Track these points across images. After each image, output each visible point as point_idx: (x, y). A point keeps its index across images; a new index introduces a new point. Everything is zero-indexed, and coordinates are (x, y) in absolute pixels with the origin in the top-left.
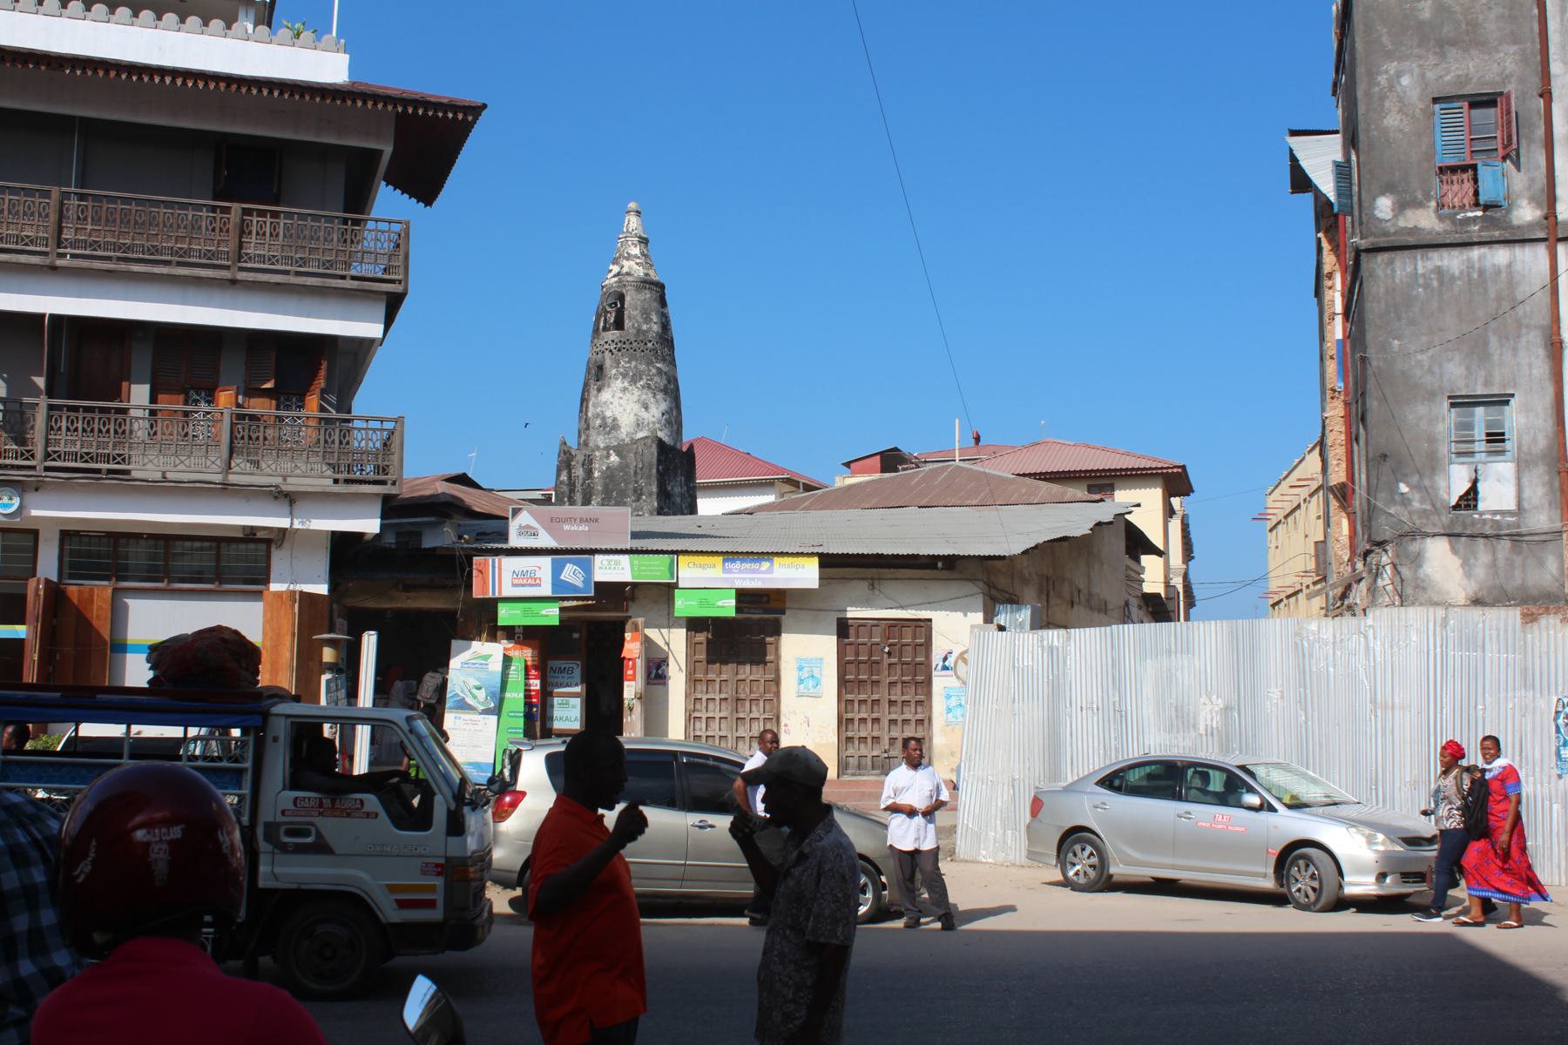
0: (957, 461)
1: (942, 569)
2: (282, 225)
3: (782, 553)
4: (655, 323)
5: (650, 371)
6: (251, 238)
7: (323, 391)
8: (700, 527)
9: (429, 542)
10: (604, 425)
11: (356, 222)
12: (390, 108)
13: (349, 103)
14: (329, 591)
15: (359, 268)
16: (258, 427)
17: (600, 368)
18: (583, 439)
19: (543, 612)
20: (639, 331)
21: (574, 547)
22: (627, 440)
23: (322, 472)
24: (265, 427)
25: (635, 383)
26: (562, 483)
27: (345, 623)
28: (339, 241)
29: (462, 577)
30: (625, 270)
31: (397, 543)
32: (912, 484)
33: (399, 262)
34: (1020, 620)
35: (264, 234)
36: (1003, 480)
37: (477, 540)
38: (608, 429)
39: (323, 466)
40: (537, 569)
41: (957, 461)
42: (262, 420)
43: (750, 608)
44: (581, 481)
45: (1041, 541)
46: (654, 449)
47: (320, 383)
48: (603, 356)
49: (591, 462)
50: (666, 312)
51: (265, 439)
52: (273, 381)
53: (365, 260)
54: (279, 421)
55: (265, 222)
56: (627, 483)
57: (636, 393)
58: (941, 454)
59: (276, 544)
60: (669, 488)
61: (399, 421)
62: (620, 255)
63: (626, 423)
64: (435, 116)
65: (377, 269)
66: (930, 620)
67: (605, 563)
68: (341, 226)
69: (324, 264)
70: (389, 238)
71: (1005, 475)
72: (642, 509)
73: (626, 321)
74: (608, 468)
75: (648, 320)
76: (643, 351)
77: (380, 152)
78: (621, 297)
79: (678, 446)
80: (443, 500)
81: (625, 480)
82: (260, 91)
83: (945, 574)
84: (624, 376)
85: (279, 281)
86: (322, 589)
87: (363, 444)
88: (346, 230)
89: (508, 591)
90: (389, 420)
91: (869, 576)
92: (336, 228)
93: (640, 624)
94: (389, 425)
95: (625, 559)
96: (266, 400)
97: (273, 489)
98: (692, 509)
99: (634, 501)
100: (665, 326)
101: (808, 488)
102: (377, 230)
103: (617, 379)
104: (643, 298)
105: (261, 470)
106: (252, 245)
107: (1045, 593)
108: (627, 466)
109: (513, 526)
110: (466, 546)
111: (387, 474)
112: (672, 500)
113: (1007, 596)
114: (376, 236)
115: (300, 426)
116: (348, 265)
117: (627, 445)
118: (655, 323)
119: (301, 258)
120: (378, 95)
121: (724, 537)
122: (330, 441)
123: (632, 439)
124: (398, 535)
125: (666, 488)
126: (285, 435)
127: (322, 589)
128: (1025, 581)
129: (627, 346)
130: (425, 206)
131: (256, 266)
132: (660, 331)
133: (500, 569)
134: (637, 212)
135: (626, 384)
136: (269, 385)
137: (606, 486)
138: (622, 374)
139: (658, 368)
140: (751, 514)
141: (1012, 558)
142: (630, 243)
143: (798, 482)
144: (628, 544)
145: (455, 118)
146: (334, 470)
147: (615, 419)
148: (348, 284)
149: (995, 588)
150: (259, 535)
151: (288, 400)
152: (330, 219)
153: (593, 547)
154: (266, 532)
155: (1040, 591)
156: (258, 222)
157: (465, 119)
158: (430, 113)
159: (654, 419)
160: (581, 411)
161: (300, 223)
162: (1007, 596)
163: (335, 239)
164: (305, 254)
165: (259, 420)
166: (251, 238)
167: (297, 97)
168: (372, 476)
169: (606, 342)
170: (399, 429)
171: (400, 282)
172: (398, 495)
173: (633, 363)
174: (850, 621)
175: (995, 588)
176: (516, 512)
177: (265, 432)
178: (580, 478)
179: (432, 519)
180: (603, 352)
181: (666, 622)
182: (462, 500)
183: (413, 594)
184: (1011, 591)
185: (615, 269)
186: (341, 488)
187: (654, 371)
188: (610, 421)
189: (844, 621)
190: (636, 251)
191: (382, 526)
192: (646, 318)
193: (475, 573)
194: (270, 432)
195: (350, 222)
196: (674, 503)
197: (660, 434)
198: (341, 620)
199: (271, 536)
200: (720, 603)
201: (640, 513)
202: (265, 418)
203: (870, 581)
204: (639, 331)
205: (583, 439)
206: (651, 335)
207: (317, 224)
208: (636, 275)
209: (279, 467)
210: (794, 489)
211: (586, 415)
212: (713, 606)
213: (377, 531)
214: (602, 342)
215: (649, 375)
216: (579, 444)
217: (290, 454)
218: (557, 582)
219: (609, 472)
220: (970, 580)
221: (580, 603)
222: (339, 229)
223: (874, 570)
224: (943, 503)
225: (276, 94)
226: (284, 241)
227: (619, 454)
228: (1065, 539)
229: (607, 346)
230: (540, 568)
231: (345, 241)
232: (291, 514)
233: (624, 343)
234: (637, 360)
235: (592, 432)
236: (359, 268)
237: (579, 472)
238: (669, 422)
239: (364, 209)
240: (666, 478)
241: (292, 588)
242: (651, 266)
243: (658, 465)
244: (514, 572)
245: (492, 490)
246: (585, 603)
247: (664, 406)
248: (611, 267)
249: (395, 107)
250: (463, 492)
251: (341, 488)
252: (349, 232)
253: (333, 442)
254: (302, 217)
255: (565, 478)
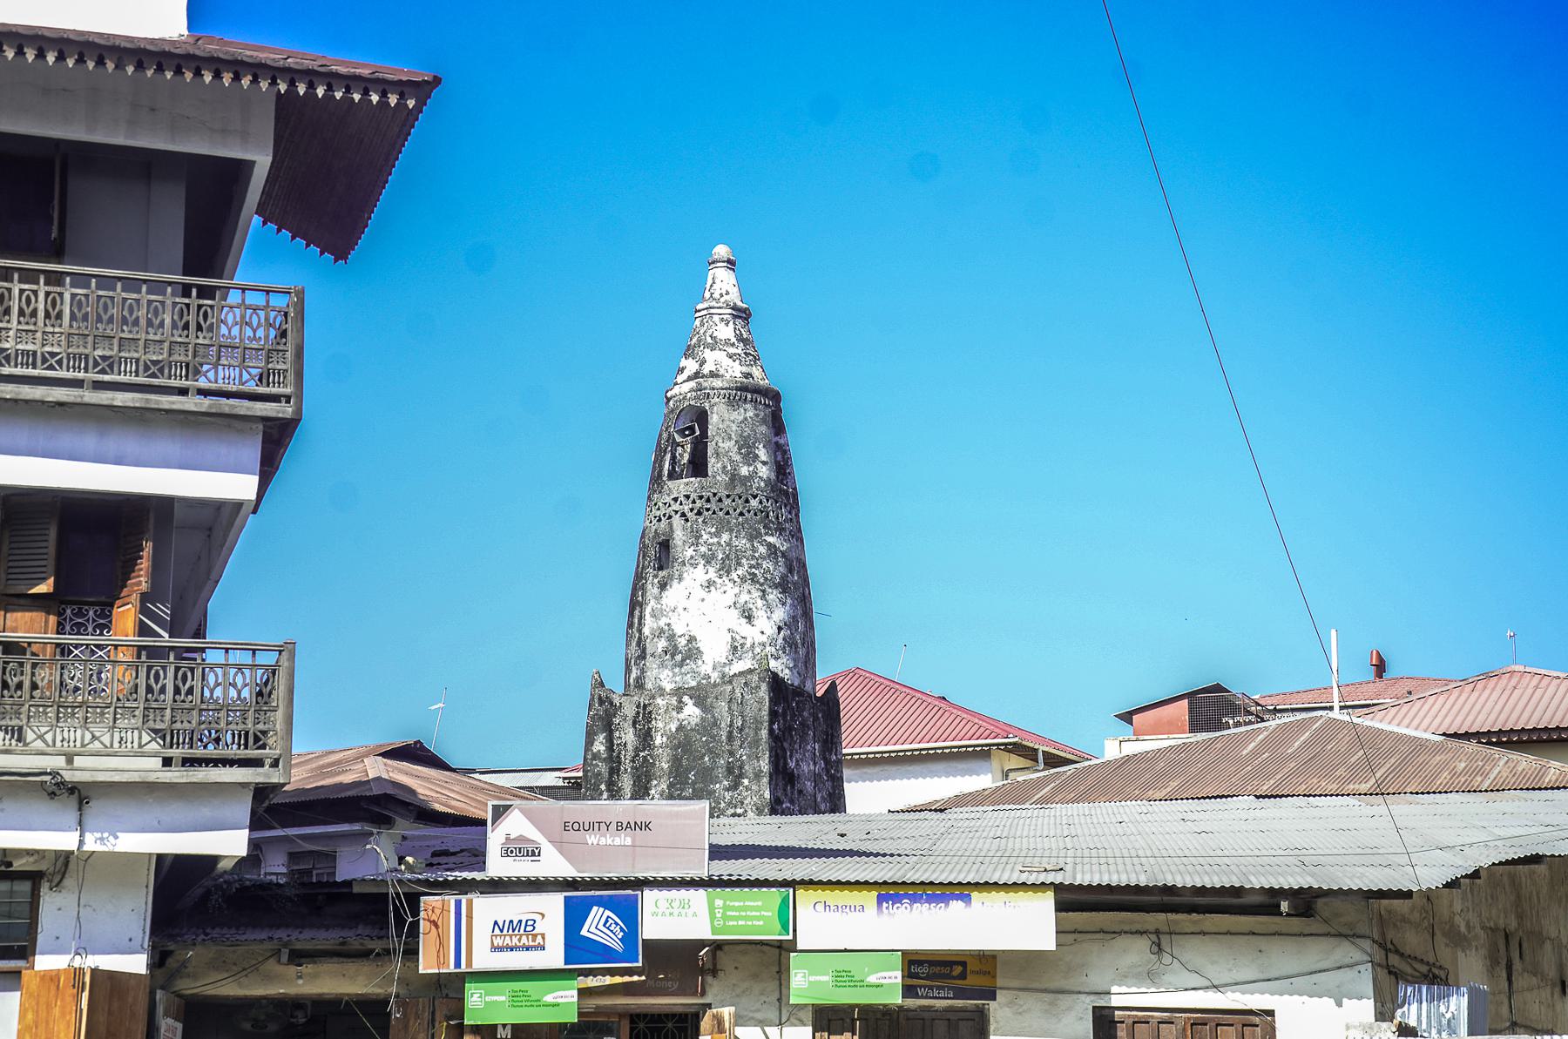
0: (1336, 708)
1: (1288, 915)
2: (67, 297)
3: (987, 883)
4: (764, 463)
5: (754, 550)
6: (8, 322)
7: (145, 598)
8: (843, 835)
9: (347, 870)
10: (672, 651)
11: (206, 292)
12: (264, 85)
13: (189, 76)
14: (151, 966)
15: (211, 375)
16: (21, 665)
17: (665, 545)
18: (633, 675)
19: (549, 998)
20: (734, 478)
21: (606, 875)
22: (715, 677)
23: (140, 746)
24: (34, 666)
25: (728, 572)
26: (596, 756)
27: (180, 1026)
28: (174, 325)
29: (399, 936)
30: (706, 370)
31: (291, 873)
32: (1245, 752)
33: (284, 364)
34: (1448, 1015)
35: (34, 313)
36: (1419, 745)
37: (430, 865)
38: (678, 658)
39: (144, 733)
40: (538, 917)
41: (1336, 708)
42: (28, 653)
43: (931, 988)
44: (630, 754)
45: (1485, 862)
46: (764, 692)
47: (140, 583)
48: (671, 525)
49: (648, 717)
50: (782, 441)
51: (34, 686)
52: (52, 580)
53: (224, 361)
54: (62, 654)
55: (35, 293)
56: (715, 755)
57: (729, 592)
58: (1310, 696)
59: (50, 881)
60: (792, 764)
61: (286, 649)
62: (699, 341)
63: (714, 651)
64: (347, 100)
65: (246, 376)
66: (1271, 1013)
67: (663, 905)
68: (177, 300)
69: (147, 368)
70: (267, 318)
71: (1428, 736)
72: (742, 803)
73: (712, 461)
74: (680, 728)
75: (750, 458)
76: (741, 514)
77: (250, 165)
78: (702, 417)
79: (808, 687)
80: (376, 791)
81: (710, 751)
82: (20, 52)
83: (1296, 924)
84: (709, 560)
85: (64, 399)
86: (136, 964)
87: (218, 692)
88: (188, 306)
89: (484, 958)
90: (267, 649)
91: (1152, 928)
92: (169, 302)
93: (726, 1018)
94: (268, 659)
95: (699, 896)
96: (37, 617)
97: (47, 778)
98: (836, 804)
99: (728, 790)
100: (782, 467)
101: (1053, 761)
102: (243, 305)
103: (695, 566)
104: (741, 418)
105: (26, 745)
106: (11, 333)
107: (1504, 963)
108: (715, 724)
109: (495, 839)
110: (408, 876)
111: (263, 747)
112: (797, 786)
113: (1424, 969)
114: (243, 317)
115: (102, 662)
116: (193, 371)
117: (715, 685)
118: (764, 463)
119: (104, 358)
120: (242, 63)
121: (884, 855)
122: (157, 688)
123: (724, 676)
124: (294, 857)
125: (786, 763)
126: (72, 679)
127: (136, 964)
128: (1459, 940)
129: (713, 505)
130: (336, 261)
131: (19, 371)
132: (773, 476)
133: (470, 917)
134: (729, 261)
135: (712, 575)
136: (44, 588)
137: (676, 761)
138: (703, 556)
139: (770, 545)
140: (941, 811)
141: (1428, 895)
142: (716, 318)
143: (1036, 750)
144: (703, 868)
145: (383, 103)
146: (164, 741)
147: (692, 639)
148: (191, 403)
149: (1397, 952)
150: (18, 865)
151: (80, 614)
152: (157, 287)
153: (641, 875)
154: (31, 859)
155: (1493, 961)
156: (22, 291)
157: (401, 104)
158: (338, 95)
159: (764, 639)
160: (630, 625)
161: (101, 293)
162: (1424, 969)
163: (168, 321)
164: (111, 349)
165: (23, 651)
166: (8, 322)
167: (91, 65)
168: (234, 751)
169: (675, 500)
170: (284, 662)
171: (288, 399)
172: (284, 785)
173: (725, 537)
174: (1117, 1013)
175: (1397, 952)
176: (499, 812)
177: (33, 674)
178: (630, 747)
179: (356, 827)
180: (670, 517)
181: (773, 1015)
182: (413, 792)
183: (308, 969)
184: (1432, 960)
185: (691, 366)
186: (176, 775)
187: (762, 550)
188: (682, 642)
189: (1106, 1012)
190: (726, 332)
191: (254, 844)
192: (749, 453)
193: (423, 926)
194: (43, 675)
195: (194, 292)
196: (800, 792)
197: (773, 664)
198: (170, 1021)
199: (42, 867)
200: (872, 979)
201: (739, 811)
202: (34, 648)
203: (1154, 937)
204: (734, 478)
205: (633, 675)
206: (758, 484)
207: (135, 296)
208: (728, 376)
209: (59, 738)
210: (1028, 763)
211: (640, 631)
212: (861, 984)
213: (243, 852)
214: (668, 499)
215: (753, 557)
216: (627, 685)
217: (80, 714)
218: (575, 944)
219: (681, 736)
220: (1346, 936)
221: (618, 980)
222: (175, 304)
223: (1162, 916)
224: (1302, 789)
225: (51, 58)
226: (71, 326)
227: (700, 702)
228: (1535, 859)
229: (676, 507)
230: (543, 916)
231: (186, 326)
232: (80, 823)
233: (708, 501)
234: (731, 531)
235: (650, 662)
236: (211, 375)
237: (628, 736)
238: (790, 643)
239: (227, 271)
240: (786, 745)
241: (78, 962)
242: (756, 359)
243: (771, 723)
244: (496, 923)
245: (474, 771)
246: (627, 979)
247: (780, 614)
248: (684, 362)
249: (274, 83)
250: (401, 771)
251: (176, 775)
252: (193, 309)
253: (163, 690)
254: (106, 282)
255: (602, 748)
